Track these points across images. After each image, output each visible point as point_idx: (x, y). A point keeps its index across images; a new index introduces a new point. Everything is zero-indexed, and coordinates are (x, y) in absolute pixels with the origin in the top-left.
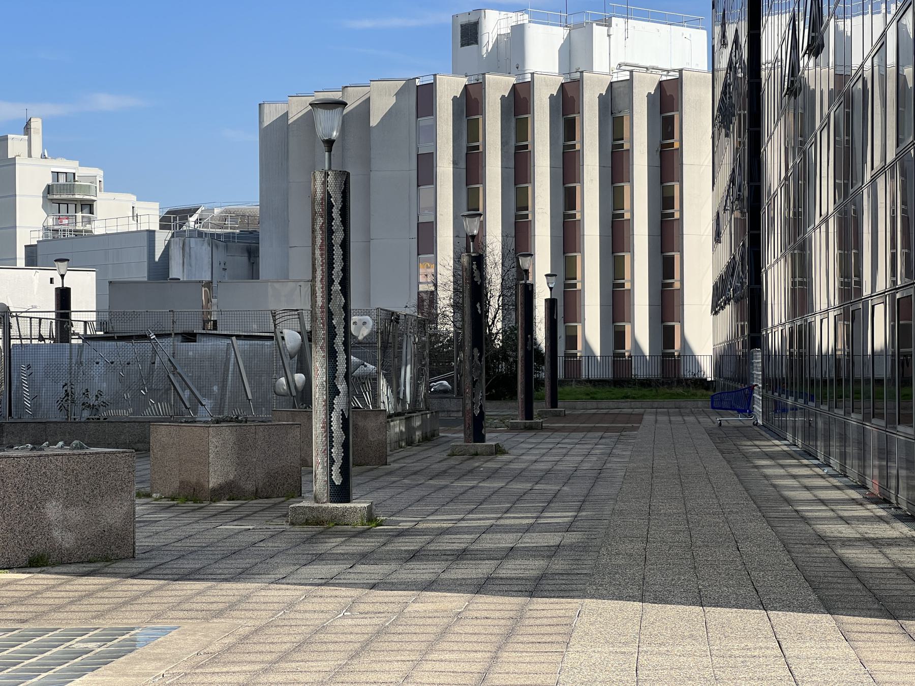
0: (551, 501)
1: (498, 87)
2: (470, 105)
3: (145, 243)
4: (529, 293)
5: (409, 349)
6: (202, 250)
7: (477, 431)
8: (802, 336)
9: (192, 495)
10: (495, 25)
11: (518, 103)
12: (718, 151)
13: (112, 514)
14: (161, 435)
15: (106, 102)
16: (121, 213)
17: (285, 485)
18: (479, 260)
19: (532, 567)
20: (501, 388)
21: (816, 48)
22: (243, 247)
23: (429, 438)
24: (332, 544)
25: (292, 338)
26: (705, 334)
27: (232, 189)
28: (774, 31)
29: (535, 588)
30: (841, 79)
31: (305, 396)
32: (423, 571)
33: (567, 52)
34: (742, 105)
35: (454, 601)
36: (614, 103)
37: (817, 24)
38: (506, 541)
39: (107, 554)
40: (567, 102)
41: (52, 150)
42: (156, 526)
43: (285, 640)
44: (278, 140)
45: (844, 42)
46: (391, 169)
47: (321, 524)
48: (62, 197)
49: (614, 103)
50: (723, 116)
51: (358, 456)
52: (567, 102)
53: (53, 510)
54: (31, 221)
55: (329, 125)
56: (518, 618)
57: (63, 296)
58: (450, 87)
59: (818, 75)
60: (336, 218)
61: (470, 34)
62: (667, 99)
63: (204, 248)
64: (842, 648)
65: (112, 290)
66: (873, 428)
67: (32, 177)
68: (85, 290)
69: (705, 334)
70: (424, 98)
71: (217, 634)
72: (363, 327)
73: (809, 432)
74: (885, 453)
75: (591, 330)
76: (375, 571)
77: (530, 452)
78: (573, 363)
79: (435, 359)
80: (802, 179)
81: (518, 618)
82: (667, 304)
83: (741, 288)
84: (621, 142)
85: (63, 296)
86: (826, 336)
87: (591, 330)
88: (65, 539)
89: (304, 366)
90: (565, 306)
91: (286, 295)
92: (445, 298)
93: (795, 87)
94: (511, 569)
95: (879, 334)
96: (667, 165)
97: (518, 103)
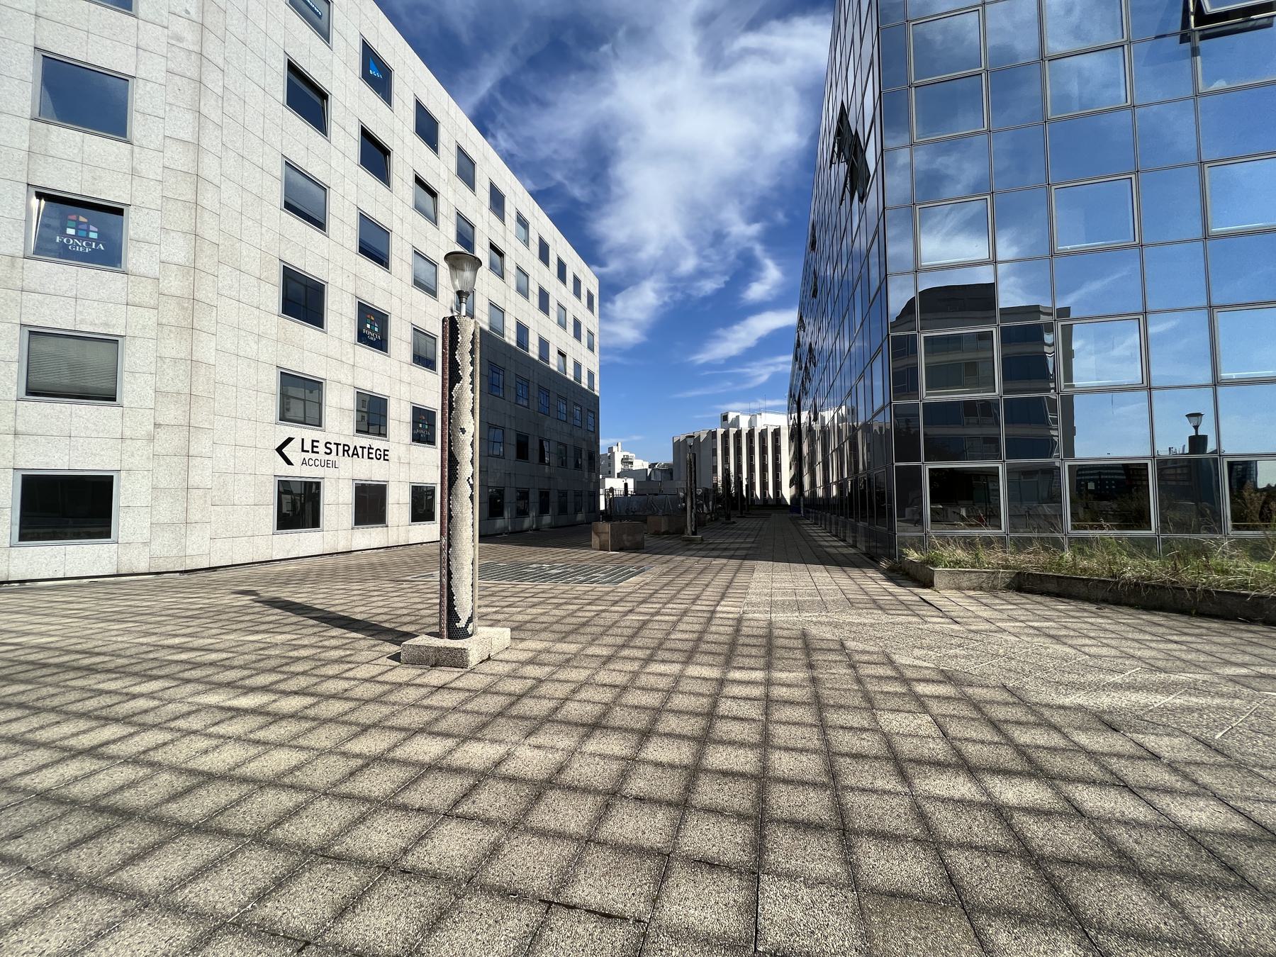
0: (748, 536)
1: (733, 431)
2: (725, 436)
3: (92, 383)
4: (741, 483)
5: (711, 496)
6: (659, 473)
7: (728, 518)
8: (813, 493)
9: (657, 534)
10: (731, 416)
11: (738, 435)
12: (87, 602)
13: (639, 538)
14: (650, 519)
15: (636, 438)
16: (639, 464)
17: (680, 531)
18: (729, 475)
19: (744, 552)
20: (735, 507)
21: (815, 419)
22: (668, 471)
23: (716, 519)
24: (693, 546)
25: (682, 494)
26: (787, 492)
27: (666, 458)
28: (804, 415)
29: (745, 558)
30: (823, 427)
31: (685, 508)
32: (716, 553)
33: (750, 422)
34: (796, 434)
35: (724, 561)
36: (763, 434)
37: (816, 414)
38: (737, 546)
39: (637, 548)
40: (750, 434)
41: (623, 450)
42: (650, 541)
43: (682, 570)
44: (678, 447)
45: (823, 418)
46: (706, 452)
47: (691, 541)
48: (626, 461)
49: (763, 434)
50: (791, 437)
51: (700, 524)
52: (750, 434)
53: (625, 537)
54: (618, 467)
55: (690, 442)
56: (740, 566)
57: (626, 485)
58: (720, 431)
59: (817, 426)
60: (693, 466)
61: (725, 418)
62: (777, 433)
63: (842, 165)
64: (826, 574)
65: (637, 484)
66: (833, 517)
67: (618, 457)
68: (631, 482)
69: (787, 492)
70: (714, 434)
71: (665, 568)
72: (700, 492)
73: (816, 518)
74: (837, 524)
75: (758, 492)
76: (703, 553)
77: (742, 523)
78: (753, 501)
79: (718, 499)
80: (813, 453)
81: (740, 566)
82: (777, 485)
83: (797, 481)
84: (570, 497)
85: (626, 485)
86: (820, 493)
87: (758, 492)
88: (628, 544)
89: (685, 501)
90: (751, 486)
91: (680, 484)
92: (720, 484)
93: (810, 429)
94: (738, 553)
95: (834, 492)
96: (777, 450)
97: (738, 435)
